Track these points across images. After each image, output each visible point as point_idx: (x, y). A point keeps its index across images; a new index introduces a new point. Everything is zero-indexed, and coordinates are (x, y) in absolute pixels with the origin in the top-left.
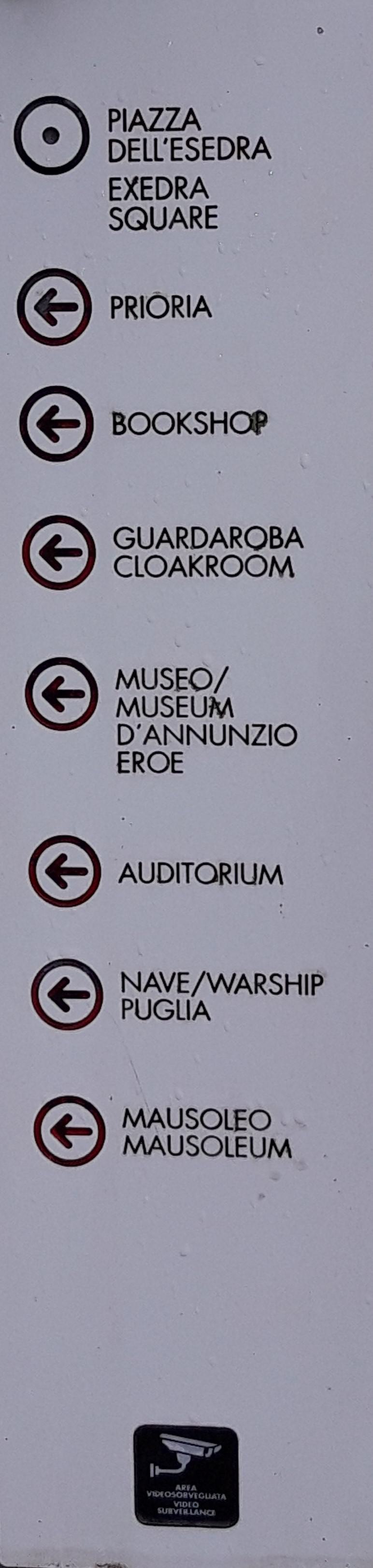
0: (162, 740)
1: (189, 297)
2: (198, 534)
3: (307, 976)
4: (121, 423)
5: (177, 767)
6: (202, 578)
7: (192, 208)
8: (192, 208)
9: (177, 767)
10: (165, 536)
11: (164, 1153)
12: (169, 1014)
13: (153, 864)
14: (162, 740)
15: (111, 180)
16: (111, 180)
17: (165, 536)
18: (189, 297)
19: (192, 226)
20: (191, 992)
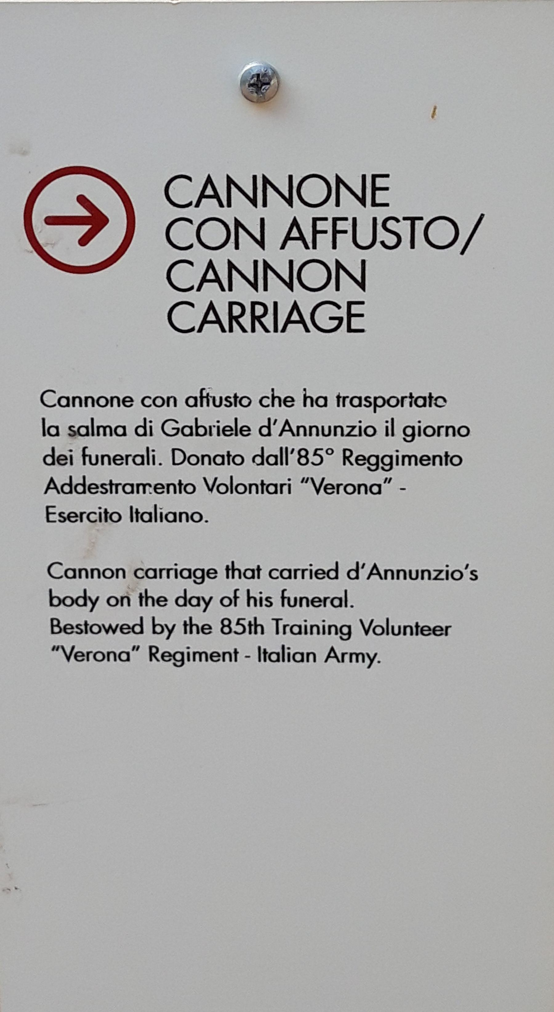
0: (226, 285)
1: (276, 304)
2: (442, 430)
3: (156, 521)
4: (58, 626)
5: (356, 323)
6: (352, 466)
7: (231, 304)
8: (231, 304)
9: (356, 323)
10: (209, 188)
11: (307, 330)
12: (335, 323)
13: (364, 177)
14: (226, 285)
15: (48, 508)
16: (48, 508)
17: (209, 188)
18: (276, 304)
19: (231, 330)
20: (271, 404)
